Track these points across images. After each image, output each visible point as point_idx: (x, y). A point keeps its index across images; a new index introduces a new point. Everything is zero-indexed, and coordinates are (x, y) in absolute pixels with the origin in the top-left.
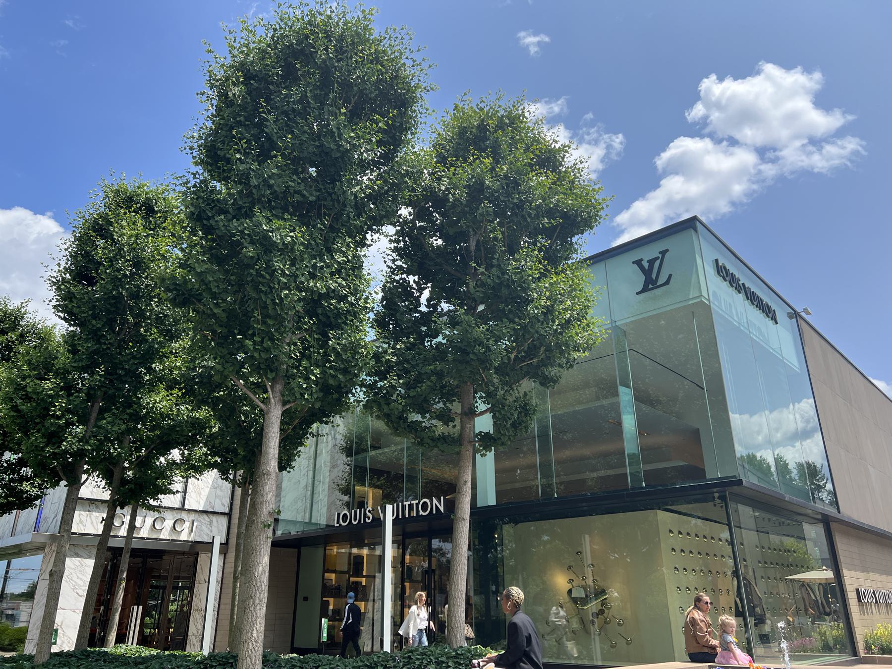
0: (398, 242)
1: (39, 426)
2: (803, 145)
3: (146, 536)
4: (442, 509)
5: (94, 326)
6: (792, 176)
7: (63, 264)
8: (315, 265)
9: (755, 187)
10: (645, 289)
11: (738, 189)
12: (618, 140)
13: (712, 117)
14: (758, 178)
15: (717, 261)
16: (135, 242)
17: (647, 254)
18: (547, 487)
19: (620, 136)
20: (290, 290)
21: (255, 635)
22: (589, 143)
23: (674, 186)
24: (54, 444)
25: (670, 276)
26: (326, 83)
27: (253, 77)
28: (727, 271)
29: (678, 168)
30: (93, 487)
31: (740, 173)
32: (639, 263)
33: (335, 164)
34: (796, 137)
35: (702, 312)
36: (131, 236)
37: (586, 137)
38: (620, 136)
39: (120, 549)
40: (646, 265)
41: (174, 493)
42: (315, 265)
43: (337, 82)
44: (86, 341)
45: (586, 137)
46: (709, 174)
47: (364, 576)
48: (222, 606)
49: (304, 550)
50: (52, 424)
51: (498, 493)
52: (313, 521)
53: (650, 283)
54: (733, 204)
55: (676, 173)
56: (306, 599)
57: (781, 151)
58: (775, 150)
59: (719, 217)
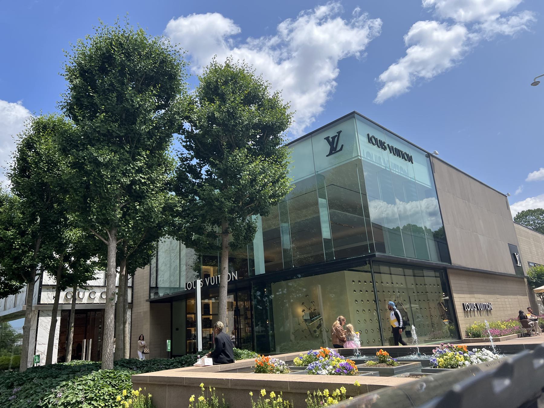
0: (186, 142)
1: (8, 254)
2: (498, 19)
3: (86, 302)
4: (236, 278)
5: (31, 199)
6: (491, 40)
7: (13, 165)
8: (126, 168)
9: (467, 48)
10: (331, 153)
11: (455, 51)
12: (377, 23)
13: (439, 4)
14: (468, 42)
15: (368, 135)
16: (48, 152)
17: (331, 133)
18: (329, 255)
19: (379, 20)
20: (111, 185)
21: (108, 351)
22: (358, 27)
23: (416, 53)
24: (17, 263)
25: (342, 145)
26: (122, 73)
27: (85, 72)
28: (376, 140)
29: (417, 41)
30: (48, 279)
31: (457, 39)
32: (327, 139)
33: (130, 116)
34: (492, 13)
35: (358, 164)
36: (46, 149)
37: (356, 24)
38: (379, 20)
39: (69, 311)
40: (331, 140)
41: (96, 279)
42: (126, 168)
43: (128, 73)
44: (29, 207)
45: (356, 24)
46: (437, 43)
47: (211, 315)
48: (132, 337)
49: (174, 303)
50: (15, 253)
51: (266, 267)
52: (181, 287)
53: (333, 150)
54: (453, 61)
55: (416, 44)
56: (177, 329)
57: (483, 24)
58: (479, 23)
59: (444, 71)
